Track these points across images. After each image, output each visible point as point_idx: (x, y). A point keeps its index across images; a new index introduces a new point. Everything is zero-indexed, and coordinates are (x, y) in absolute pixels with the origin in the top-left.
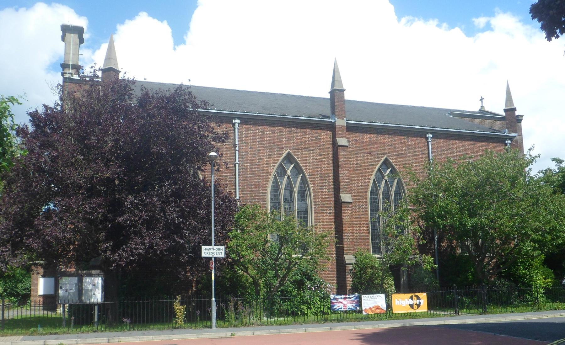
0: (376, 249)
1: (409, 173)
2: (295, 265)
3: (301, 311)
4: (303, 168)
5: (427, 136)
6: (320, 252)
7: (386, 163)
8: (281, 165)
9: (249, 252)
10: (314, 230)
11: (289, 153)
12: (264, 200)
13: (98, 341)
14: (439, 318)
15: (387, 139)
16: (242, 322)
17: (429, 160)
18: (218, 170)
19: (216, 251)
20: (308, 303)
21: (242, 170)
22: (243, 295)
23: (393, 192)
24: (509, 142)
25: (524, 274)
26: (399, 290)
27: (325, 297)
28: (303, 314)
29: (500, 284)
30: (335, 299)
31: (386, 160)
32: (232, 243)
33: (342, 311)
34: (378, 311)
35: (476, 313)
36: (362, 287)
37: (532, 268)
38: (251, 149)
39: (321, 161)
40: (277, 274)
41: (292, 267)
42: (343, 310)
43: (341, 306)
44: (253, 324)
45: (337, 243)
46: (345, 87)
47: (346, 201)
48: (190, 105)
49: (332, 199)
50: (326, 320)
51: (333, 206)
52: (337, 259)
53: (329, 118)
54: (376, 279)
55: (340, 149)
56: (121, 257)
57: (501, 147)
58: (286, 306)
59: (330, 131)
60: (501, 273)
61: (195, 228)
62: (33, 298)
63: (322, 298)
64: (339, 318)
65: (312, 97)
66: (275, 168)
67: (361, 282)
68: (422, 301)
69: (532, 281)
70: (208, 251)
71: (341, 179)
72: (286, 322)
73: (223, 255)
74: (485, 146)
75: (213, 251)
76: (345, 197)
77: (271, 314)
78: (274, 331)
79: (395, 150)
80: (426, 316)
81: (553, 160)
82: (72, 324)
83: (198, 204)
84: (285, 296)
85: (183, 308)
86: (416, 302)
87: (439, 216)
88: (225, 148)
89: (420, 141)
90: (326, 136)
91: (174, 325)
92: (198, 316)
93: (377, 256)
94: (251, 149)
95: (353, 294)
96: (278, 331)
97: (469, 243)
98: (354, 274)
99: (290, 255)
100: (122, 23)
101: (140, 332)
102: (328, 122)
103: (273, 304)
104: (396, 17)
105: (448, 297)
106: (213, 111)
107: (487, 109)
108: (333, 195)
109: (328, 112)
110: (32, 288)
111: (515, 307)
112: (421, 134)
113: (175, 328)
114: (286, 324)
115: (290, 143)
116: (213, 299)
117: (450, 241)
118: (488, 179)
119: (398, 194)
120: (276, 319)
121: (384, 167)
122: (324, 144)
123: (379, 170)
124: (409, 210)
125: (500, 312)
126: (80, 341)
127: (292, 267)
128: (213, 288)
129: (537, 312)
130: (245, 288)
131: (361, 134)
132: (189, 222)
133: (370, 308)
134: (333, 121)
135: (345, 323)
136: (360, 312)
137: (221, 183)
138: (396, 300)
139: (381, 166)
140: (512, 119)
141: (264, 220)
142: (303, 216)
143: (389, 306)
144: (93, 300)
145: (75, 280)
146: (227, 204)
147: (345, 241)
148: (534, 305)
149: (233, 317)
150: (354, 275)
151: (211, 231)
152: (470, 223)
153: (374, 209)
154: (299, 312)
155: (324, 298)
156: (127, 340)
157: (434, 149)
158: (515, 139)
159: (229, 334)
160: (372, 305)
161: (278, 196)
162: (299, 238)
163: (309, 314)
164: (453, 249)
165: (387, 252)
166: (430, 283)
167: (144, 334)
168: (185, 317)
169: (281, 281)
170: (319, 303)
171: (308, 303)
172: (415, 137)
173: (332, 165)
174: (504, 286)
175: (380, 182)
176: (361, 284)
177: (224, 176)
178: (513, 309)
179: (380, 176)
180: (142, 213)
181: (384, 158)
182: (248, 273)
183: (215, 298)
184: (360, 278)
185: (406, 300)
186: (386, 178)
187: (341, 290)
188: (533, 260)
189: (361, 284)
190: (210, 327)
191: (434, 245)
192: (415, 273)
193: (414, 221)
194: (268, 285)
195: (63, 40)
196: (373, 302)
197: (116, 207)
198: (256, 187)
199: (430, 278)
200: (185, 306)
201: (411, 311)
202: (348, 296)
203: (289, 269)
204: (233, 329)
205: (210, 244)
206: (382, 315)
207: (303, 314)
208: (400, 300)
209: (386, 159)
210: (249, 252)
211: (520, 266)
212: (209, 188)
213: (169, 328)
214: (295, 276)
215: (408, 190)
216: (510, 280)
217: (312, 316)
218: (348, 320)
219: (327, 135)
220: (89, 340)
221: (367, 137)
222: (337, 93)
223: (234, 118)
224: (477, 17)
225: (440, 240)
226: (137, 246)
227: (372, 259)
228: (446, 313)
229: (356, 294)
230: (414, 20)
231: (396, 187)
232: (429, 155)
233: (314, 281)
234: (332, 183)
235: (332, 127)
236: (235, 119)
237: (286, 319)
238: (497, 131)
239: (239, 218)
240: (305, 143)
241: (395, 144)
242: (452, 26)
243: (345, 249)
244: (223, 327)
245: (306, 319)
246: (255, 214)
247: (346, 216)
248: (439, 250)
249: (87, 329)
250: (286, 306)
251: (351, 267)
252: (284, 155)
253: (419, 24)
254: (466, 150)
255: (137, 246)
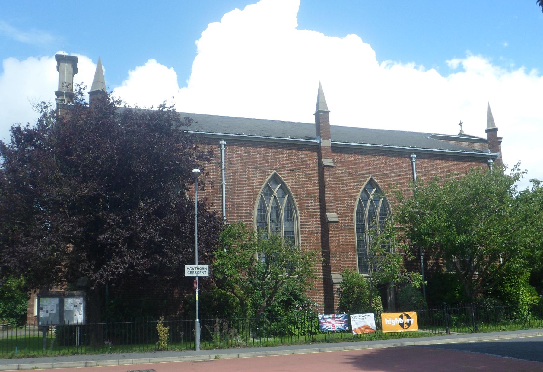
0: (363, 268)
1: (394, 192)
2: (282, 284)
3: (289, 331)
4: (290, 189)
5: (411, 156)
6: (308, 272)
7: (372, 184)
8: (267, 185)
9: (234, 271)
10: (300, 249)
11: (275, 174)
12: (251, 220)
13: (74, 365)
14: (430, 338)
15: (372, 159)
16: (227, 343)
17: (414, 179)
18: (203, 189)
19: (199, 271)
20: (296, 323)
21: (227, 189)
22: (230, 315)
23: (378, 212)
24: (492, 161)
25: (510, 291)
26: (386, 309)
27: (313, 317)
28: (291, 334)
29: (487, 302)
30: (323, 318)
31: (371, 180)
32: (216, 262)
33: (330, 331)
34: (368, 330)
35: (466, 332)
36: (349, 306)
37: (518, 285)
38: (237, 169)
39: (307, 181)
40: (263, 294)
41: (279, 287)
42: (332, 330)
43: (330, 326)
44: (239, 346)
45: (324, 262)
46: (329, 109)
47: (332, 220)
48: (174, 123)
49: (319, 218)
50: (314, 341)
51: (320, 226)
52: (324, 278)
53: (314, 139)
54: (363, 298)
55: (325, 169)
56: (102, 276)
57: (484, 166)
58: (274, 326)
59: (316, 152)
60: (487, 291)
61: (178, 246)
62: (30, 319)
63: (310, 318)
64: (327, 338)
65: (297, 123)
66: (262, 189)
67: (348, 301)
68: (412, 320)
69: (519, 299)
70: (192, 271)
71: (327, 199)
72: (273, 343)
73: (207, 274)
74: (469, 166)
75: (196, 271)
76: (332, 216)
77: (259, 335)
78: (260, 353)
79: (380, 170)
80: (417, 335)
81: (531, 181)
82: (52, 346)
83: (182, 223)
84: (273, 316)
85: (166, 329)
86: (406, 321)
87: (427, 234)
88: (210, 167)
89: (404, 161)
90: (311, 157)
91: (157, 347)
92: (182, 338)
93: (364, 275)
94: (237, 169)
95: (341, 314)
96: (264, 353)
97: (455, 260)
98: (341, 293)
99: (276, 274)
100: (133, 69)
101: (121, 355)
102: (315, 147)
103: (261, 324)
104: (377, 62)
105: (436, 315)
106: (200, 132)
107: (466, 132)
108: (319, 214)
109: (314, 134)
110: (29, 309)
111: (505, 324)
112: (405, 154)
113: (158, 350)
114: (273, 345)
115: (276, 164)
116: (197, 320)
117: (437, 260)
118: (475, 197)
119: (384, 213)
120: (262, 339)
121: (369, 187)
122: (309, 165)
123: (364, 190)
124: (396, 228)
125: (492, 331)
126: (56, 365)
127: (279, 287)
128: (197, 308)
129: (529, 330)
130: (232, 308)
131: (346, 155)
132: (173, 241)
133: (360, 328)
134: (318, 142)
135: (334, 344)
136: (350, 331)
137: (207, 202)
138: (386, 319)
139: (366, 186)
140: (493, 140)
141: (250, 239)
142: (290, 236)
143: (379, 325)
144: (75, 322)
145: (56, 301)
146: (211, 223)
147: (332, 260)
148: (524, 324)
149: (218, 338)
150: (342, 295)
151: (194, 249)
152: (459, 239)
153: (361, 229)
154: (287, 332)
155: (312, 318)
156: (105, 364)
157: (419, 169)
158: (498, 158)
159: (213, 357)
160: (361, 325)
161: (264, 217)
162: (285, 256)
163: (297, 334)
164: (439, 267)
165: (374, 270)
166: (417, 302)
167: (124, 357)
168: (168, 339)
169: (267, 300)
170: (307, 322)
171: (296, 323)
172: (399, 157)
173: (317, 185)
174: (490, 303)
175: (365, 202)
176: (349, 303)
177: (211, 198)
178: (504, 327)
179: (366, 196)
180: (123, 230)
181: (369, 178)
182: (235, 294)
183: (199, 318)
184: (347, 297)
185: (396, 319)
186: (372, 198)
187: (329, 310)
188: (518, 277)
189: (349, 303)
190: (194, 349)
191: (420, 263)
192: (402, 291)
193: (400, 240)
194: (255, 305)
195: (58, 70)
196: (362, 321)
197: (98, 225)
198: (242, 207)
199: (418, 296)
200: (168, 328)
201: (401, 330)
202: (336, 316)
203: (275, 289)
204: (218, 350)
205: (194, 263)
206: (371, 335)
207: (291, 334)
208: (390, 319)
209: (371, 179)
210: (234, 271)
211: (506, 283)
212: (193, 207)
213: (151, 351)
214: (283, 295)
215: (394, 208)
216: (496, 297)
217: (300, 335)
218: (337, 340)
219: (312, 156)
220: (66, 364)
221: (352, 158)
222: (322, 115)
223: (221, 140)
224: (450, 59)
225: (426, 259)
226: (117, 266)
227: (359, 278)
228: (437, 332)
229: (344, 313)
230: (393, 64)
231: (382, 207)
232: (413, 175)
233: (302, 301)
234: (318, 203)
235: (317, 148)
236: (221, 141)
237: (273, 339)
238: (480, 151)
239: (224, 236)
240: (291, 163)
241: (380, 164)
242: (428, 67)
243: (332, 268)
244: (207, 349)
245: (294, 340)
246: (240, 233)
247: (333, 235)
248: (425, 268)
249: (67, 352)
250: (274, 326)
251: (338, 286)
252: (271, 176)
253: (398, 67)
254: (449, 170)
255: (117, 266)
